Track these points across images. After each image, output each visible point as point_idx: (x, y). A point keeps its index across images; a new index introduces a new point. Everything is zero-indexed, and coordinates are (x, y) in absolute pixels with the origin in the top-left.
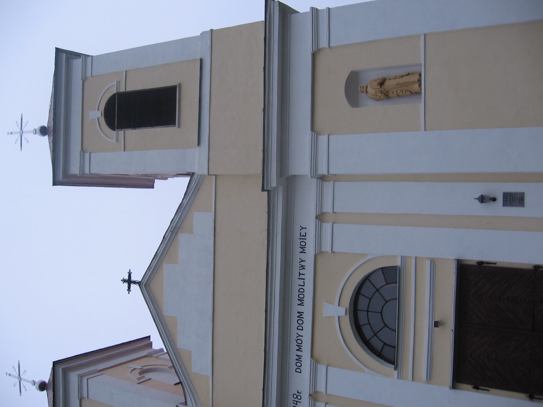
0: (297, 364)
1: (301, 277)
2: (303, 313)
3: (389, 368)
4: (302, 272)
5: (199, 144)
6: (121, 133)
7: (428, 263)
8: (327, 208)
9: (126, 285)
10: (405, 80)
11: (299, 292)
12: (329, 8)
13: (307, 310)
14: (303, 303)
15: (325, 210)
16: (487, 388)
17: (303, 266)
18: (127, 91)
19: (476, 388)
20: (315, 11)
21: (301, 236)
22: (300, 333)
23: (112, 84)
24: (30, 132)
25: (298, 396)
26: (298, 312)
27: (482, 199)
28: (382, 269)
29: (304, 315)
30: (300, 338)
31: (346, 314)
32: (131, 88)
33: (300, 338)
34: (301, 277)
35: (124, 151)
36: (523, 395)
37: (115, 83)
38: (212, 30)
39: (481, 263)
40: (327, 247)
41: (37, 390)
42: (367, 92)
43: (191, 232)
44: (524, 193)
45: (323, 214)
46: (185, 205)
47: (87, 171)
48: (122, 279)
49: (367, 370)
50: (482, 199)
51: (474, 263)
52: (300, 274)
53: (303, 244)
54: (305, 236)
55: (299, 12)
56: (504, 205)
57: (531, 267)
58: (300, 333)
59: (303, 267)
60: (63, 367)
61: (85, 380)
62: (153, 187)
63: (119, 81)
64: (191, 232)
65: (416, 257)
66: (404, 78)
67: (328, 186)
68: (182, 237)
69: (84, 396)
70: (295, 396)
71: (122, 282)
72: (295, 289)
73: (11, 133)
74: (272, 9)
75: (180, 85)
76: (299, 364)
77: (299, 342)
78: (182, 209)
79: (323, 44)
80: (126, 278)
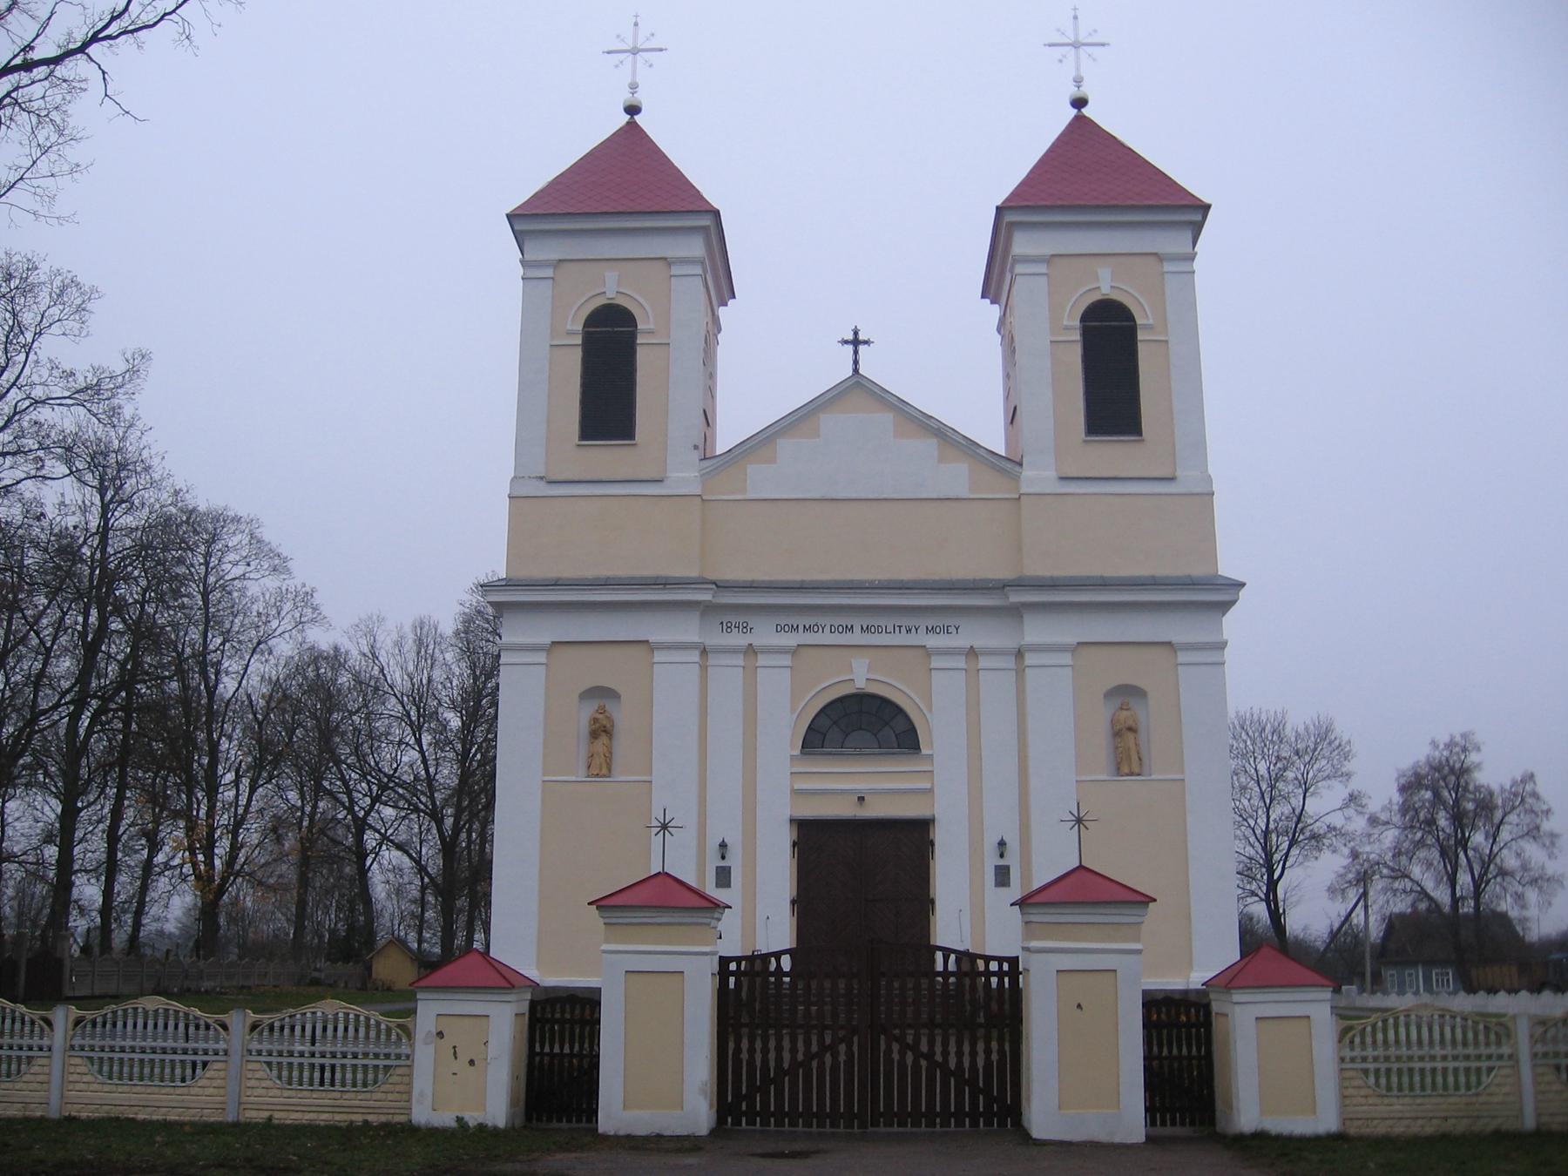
0: (786, 627)
1: (897, 629)
4: (903, 629)
5: (1062, 478)
6: (1077, 336)
8: (984, 662)
10: (1135, 757)
12: (1224, 664)
13: (857, 638)
17: (910, 630)
19: (794, 844)
20: (1221, 646)
22: (827, 629)
25: (746, 629)
26: (852, 626)
27: (1002, 844)
32: (1142, 350)
34: (897, 629)
35: (1051, 342)
36: (795, 893)
37: (1151, 321)
38: (1213, 494)
39: (932, 843)
40: (936, 662)
42: (1122, 709)
43: (941, 459)
44: (1009, 886)
47: (1019, 269)
51: (931, 837)
56: (996, 866)
58: (827, 629)
64: (941, 459)
65: (669, 344)
67: (1010, 662)
68: (931, 445)
72: (882, 621)
75: (1143, 440)
80: (861, 337)
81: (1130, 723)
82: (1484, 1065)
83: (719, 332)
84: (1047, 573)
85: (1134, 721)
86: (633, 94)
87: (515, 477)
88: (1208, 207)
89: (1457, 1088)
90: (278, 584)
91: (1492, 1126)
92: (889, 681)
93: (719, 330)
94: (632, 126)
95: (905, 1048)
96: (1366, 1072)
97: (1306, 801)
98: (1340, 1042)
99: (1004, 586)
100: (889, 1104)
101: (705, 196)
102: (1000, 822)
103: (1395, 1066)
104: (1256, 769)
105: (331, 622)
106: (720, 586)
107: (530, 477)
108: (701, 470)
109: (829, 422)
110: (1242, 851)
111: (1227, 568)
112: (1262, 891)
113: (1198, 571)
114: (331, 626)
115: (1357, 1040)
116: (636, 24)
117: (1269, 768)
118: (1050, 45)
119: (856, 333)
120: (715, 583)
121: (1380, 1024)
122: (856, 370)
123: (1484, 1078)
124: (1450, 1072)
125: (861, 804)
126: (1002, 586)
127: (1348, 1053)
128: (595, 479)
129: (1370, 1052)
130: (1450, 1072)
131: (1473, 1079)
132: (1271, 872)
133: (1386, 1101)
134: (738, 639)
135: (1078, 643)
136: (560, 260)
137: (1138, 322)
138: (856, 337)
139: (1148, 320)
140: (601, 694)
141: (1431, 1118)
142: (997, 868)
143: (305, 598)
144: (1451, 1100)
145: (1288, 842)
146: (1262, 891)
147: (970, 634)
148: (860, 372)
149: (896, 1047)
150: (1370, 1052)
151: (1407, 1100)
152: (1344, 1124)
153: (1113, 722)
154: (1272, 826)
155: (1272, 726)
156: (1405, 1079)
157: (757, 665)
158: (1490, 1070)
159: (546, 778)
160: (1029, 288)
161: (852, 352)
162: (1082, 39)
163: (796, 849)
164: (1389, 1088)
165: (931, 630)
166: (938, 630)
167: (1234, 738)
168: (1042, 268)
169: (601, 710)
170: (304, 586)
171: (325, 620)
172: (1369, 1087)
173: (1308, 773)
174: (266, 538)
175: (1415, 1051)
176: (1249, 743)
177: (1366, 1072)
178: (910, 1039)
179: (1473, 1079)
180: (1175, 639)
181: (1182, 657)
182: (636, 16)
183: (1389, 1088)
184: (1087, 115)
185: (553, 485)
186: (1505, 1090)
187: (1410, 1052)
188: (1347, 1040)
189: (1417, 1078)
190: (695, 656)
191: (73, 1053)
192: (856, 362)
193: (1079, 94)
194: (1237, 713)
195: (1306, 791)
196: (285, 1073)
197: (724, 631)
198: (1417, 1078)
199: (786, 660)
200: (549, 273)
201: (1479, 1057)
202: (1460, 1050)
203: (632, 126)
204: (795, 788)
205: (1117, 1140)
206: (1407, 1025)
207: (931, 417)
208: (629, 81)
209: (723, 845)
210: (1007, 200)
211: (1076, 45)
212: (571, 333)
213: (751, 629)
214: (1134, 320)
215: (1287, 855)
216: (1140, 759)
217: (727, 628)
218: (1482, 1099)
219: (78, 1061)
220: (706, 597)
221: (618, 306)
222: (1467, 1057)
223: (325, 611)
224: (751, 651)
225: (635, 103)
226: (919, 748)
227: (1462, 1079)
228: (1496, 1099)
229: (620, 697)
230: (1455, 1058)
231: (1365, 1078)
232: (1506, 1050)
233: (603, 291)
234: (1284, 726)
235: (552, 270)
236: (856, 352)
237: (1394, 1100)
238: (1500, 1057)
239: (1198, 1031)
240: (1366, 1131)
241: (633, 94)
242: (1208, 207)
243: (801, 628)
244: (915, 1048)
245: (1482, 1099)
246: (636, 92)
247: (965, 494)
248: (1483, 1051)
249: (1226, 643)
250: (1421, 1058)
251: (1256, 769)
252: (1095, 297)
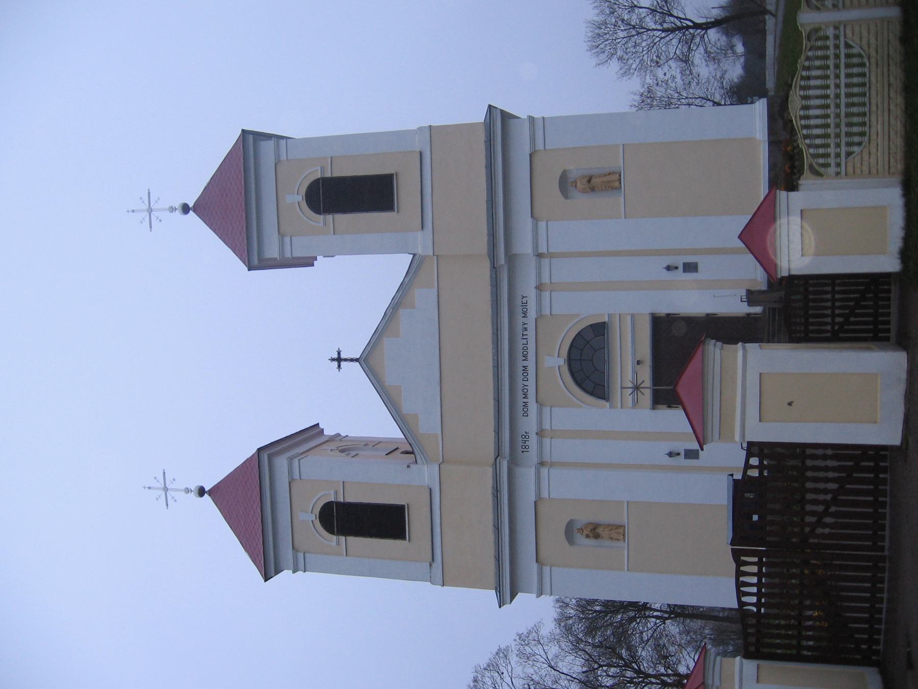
1: (525, 337)
3: (602, 402)
6: (330, 217)
7: (629, 318)
8: (546, 279)
9: (336, 363)
12: (544, 118)
13: (531, 364)
15: (543, 281)
16: (677, 406)
17: (525, 328)
19: (669, 407)
20: (532, 119)
22: (525, 383)
23: (315, 169)
24: (165, 210)
25: (526, 436)
26: (524, 367)
27: (668, 268)
28: (591, 325)
30: (525, 387)
31: (565, 363)
32: (337, 174)
33: (525, 387)
34: (525, 337)
39: (668, 315)
41: (196, 497)
42: (576, 186)
44: (697, 263)
45: (541, 284)
48: (330, 358)
49: (583, 405)
50: (668, 268)
52: (523, 335)
53: (525, 310)
54: (527, 303)
55: (518, 118)
57: (704, 315)
58: (525, 383)
59: (526, 329)
60: (268, 453)
61: (296, 462)
62: (313, 266)
66: (606, 177)
67: (545, 262)
69: (295, 478)
70: (523, 437)
71: (330, 361)
73: (133, 211)
74: (495, 115)
76: (525, 410)
77: (525, 391)
78: (404, 286)
80: (336, 356)
81: (585, 181)
82: (843, 51)
83: (340, 435)
84: (486, 238)
85: (584, 178)
86: (192, 491)
87: (430, 581)
88: (243, 130)
89: (863, 75)
90: (514, 656)
91: (896, 44)
92: (558, 347)
93: (338, 435)
94: (211, 493)
95: (819, 523)
96: (849, 154)
97: (643, 6)
99: (494, 268)
100: (865, 504)
101: (250, 456)
102: (654, 268)
103: (844, 129)
104: (623, 38)
105: (538, 622)
106: (498, 454)
107: (430, 573)
108: (423, 463)
109: (390, 380)
110: (675, 47)
111: (479, 117)
112: (700, 32)
113: (481, 136)
114: (540, 622)
115: (821, 161)
116: (149, 488)
117: (622, 30)
118: (151, 227)
119: (333, 360)
120: (496, 459)
121: (807, 141)
122: (357, 360)
123: (854, 51)
124: (849, 80)
125: (642, 363)
126: (494, 268)
127: (832, 170)
128: (430, 531)
129: (832, 150)
130: (849, 80)
131: (855, 60)
132: (688, 27)
133: (874, 137)
134: (533, 441)
135: (532, 217)
136: (293, 548)
137: (320, 176)
138: (335, 360)
139: (318, 170)
140: (570, 531)
141: (889, 98)
142: (684, 271)
143: (523, 639)
144: (873, 80)
145: (670, 17)
146: (700, 32)
147: (527, 287)
148: (358, 357)
149: (819, 531)
150: (832, 150)
151: (873, 119)
152: (893, 174)
153: (584, 191)
154: (659, 27)
155: (596, 29)
156: (855, 120)
157: (550, 429)
158: (848, 46)
159: (626, 570)
160: (299, 247)
161: (345, 358)
162: (146, 207)
163: (673, 406)
164: (862, 134)
165: (525, 315)
166: (525, 310)
167: (603, 52)
168: (287, 240)
169: (581, 530)
170: (515, 640)
171: (537, 625)
172: (862, 151)
173: (625, 6)
174: (487, 661)
175: (831, 111)
176: (607, 43)
177: (849, 154)
178: (813, 519)
179: (855, 60)
180: (527, 151)
181: (540, 146)
182: (145, 488)
183: (862, 134)
184: (193, 204)
185: (435, 558)
186: (865, 32)
187: (832, 116)
188: (822, 170)
189: (855, 110)
190: (544, 471)
192: (352, 360)
193: (180, 209)
194: (587, 51)
195: (636, 6)
198: (855, 110)
199: (547, 410)
201: (837, 56)
202: (830, 72)
203: (211, 493)
204: (632, 406)
205: (904, 376)
207: (385, 313)
208: (183, 493)
209: (671, 454)
210: (244, 263)
211: (150, 210)
212: (338, 543)
213: (526, 433)
214: (319, 179)
215: (677, 18)
216: (610, 174)
217: (525, 448)
218: (873, 53)
220: (505, 464)
222: (837, 66)
223: (530, 625)
224: (540, 434)
225: (197, 491)
226: (605, 322)
227: (855, 70)
228: (873, 41)
229: (572, 520)
230: (837, 76)
231: (854, 155)
232: (830, 32)
233: (311, 522)
234: (595, 22)
235: (299, 553)
236: (346, 360)
237: (873, 130)
238: (837, 37)
239: (812, 324)
240: (900, 155)
241: (192, 491)
242: (243, 130)
243: (525, 400)
244: (820, 516)
245: (873, 53)
246: (191, 490)
247: (435, 290)
248: (831, 52)
249: (529, 116)
250: (838, 106)
251: (623, 38)
252: (304, 205)
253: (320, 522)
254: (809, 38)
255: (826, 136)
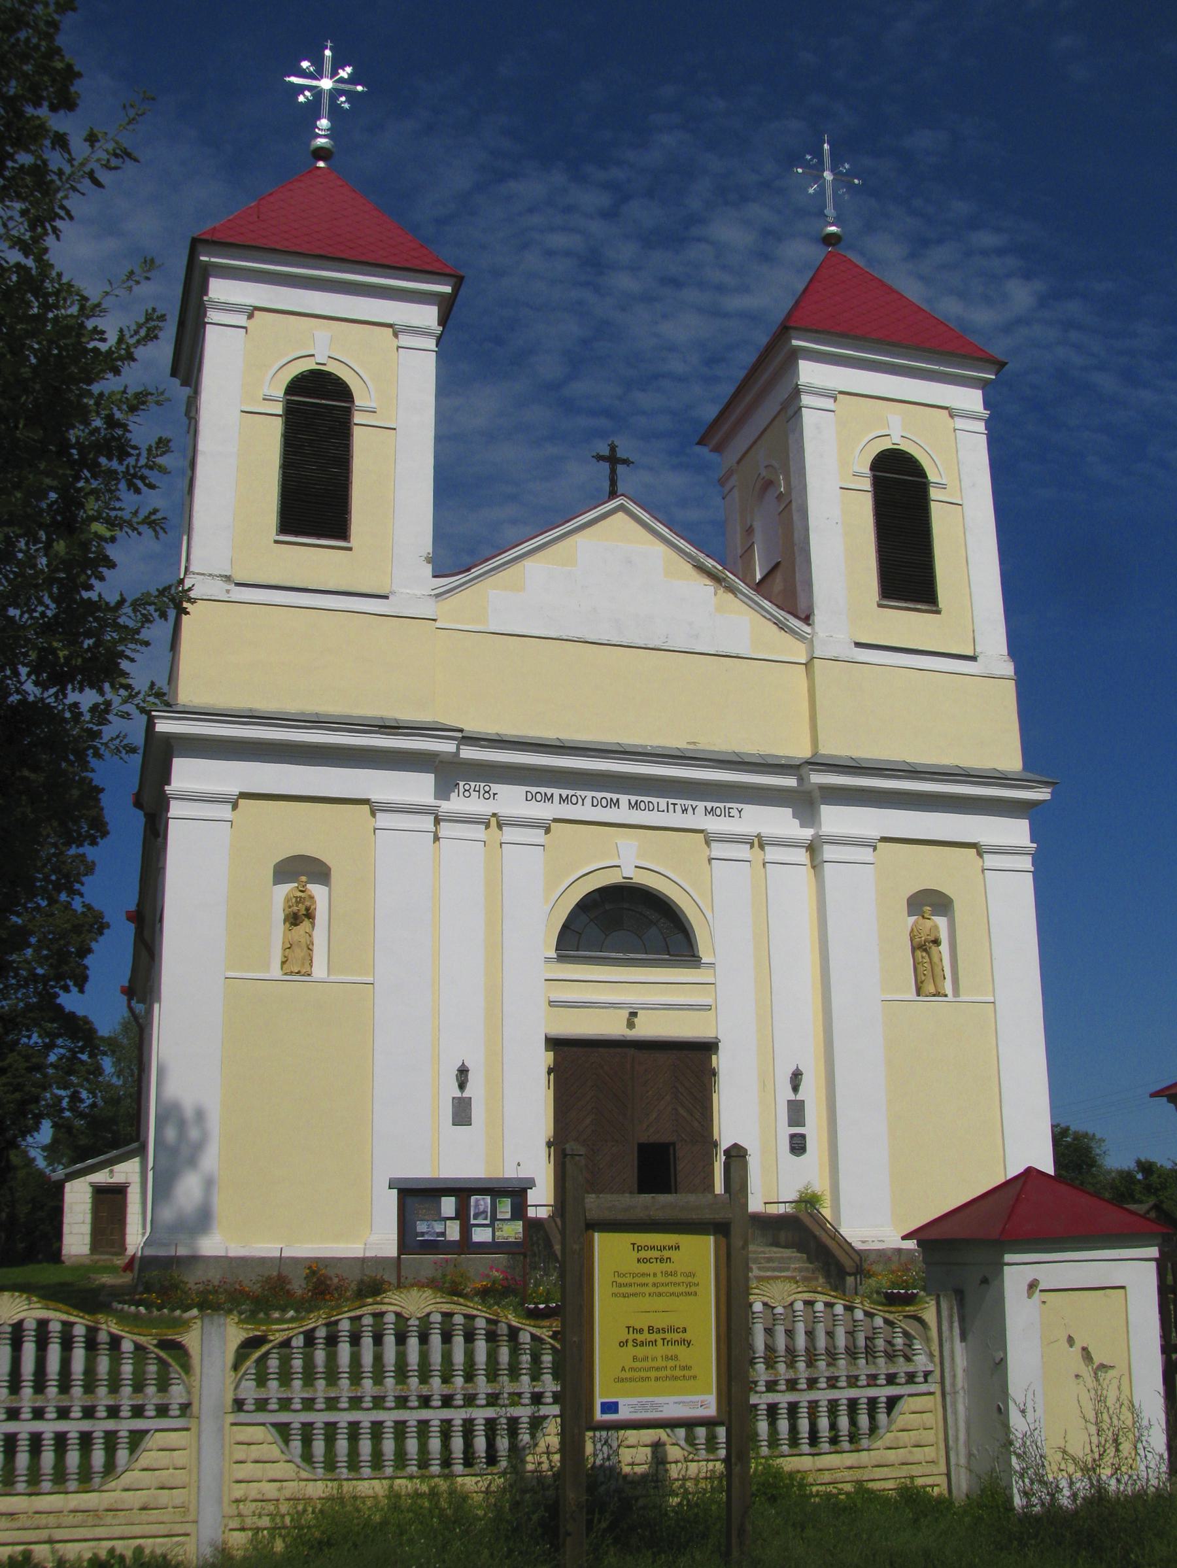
1: (671, 807)
2: (618, 808)
6: (867, 484)
11: (649, 802)
13: (623, 814)
14: (633, 808)
17: (686, 810)
18: (932, 503)
21: (729, 808)
29: (614, 809)
30: (580, 801)
31: (624, 878)
33: (580, 801)
34: (671, 807)
36: (551, 1132)
39: (714, 1073)
40: (718, 850)
46: (760, 602)
49: (548, 908)
54: (729, 816)
59: (685, 811)
63: (945, 488)
67: (802, 856)
74: (1040, 790)
79: (991, 861)
98: (236, 1367)
115: (273, 1364)
137: (357, 403)
166: (718, 813)
191: (243, 1418)
196: (319, 1447)
197: (461, 794)
200: (241, 320)
206: (378, 1340)
214: (353, 402)
219: (258, 1433)
221: (330, 374)
236: (613, 472)
243: (556, 798)
252: (886, 445)
253: (312, 372)
254: (164, 1345)
255: (402, 1373)
